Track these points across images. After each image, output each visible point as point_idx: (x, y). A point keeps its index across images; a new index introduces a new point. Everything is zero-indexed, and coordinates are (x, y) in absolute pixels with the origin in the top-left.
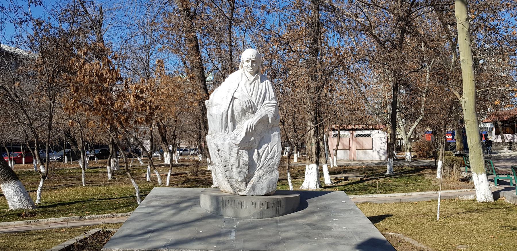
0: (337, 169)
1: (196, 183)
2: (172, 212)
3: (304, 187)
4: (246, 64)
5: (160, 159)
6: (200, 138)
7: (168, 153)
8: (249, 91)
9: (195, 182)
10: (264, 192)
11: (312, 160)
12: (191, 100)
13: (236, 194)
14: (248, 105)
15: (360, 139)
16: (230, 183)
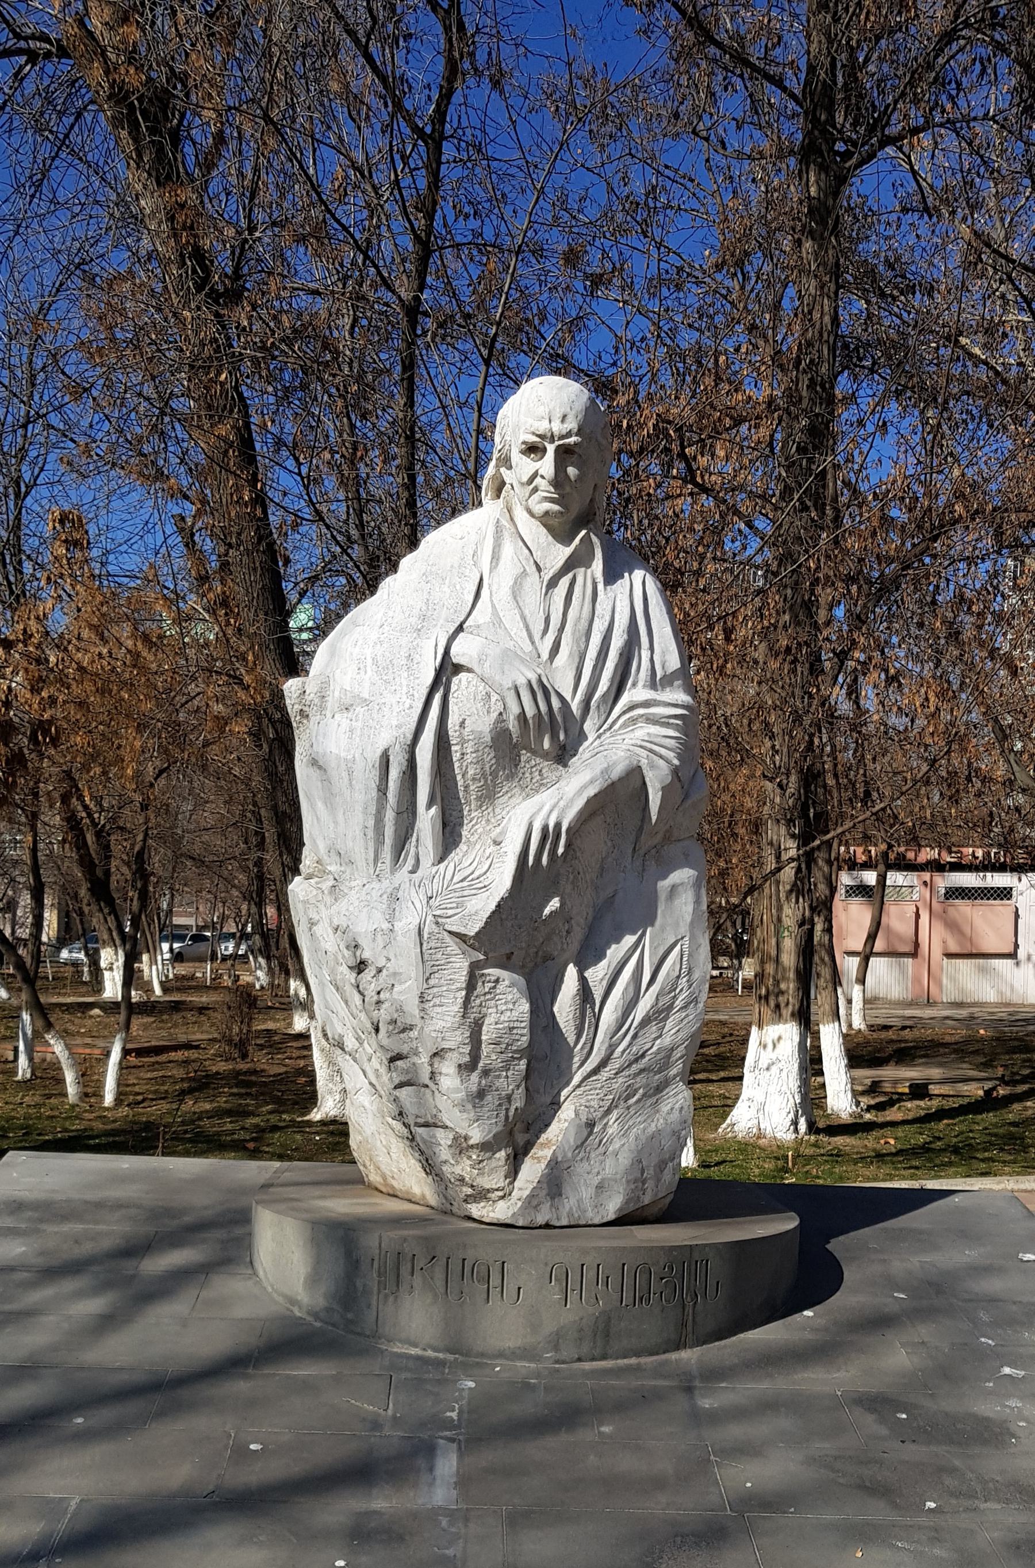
0: (868, 1042)
1: (240, 1095)
2: (94, 1306)
3: (736, 1128)
4: (524, 466)
5: (86, 977)
6: (261, 891)
7: (116, 954)
8: (537, 628)
9: (235, 1090)
10: (612, 1208)
11: (778, 1006)
12: (218, 708)
13: (452, 1214)
14: (530, 711)
15: (963, 907)
16: (422, 1153)
